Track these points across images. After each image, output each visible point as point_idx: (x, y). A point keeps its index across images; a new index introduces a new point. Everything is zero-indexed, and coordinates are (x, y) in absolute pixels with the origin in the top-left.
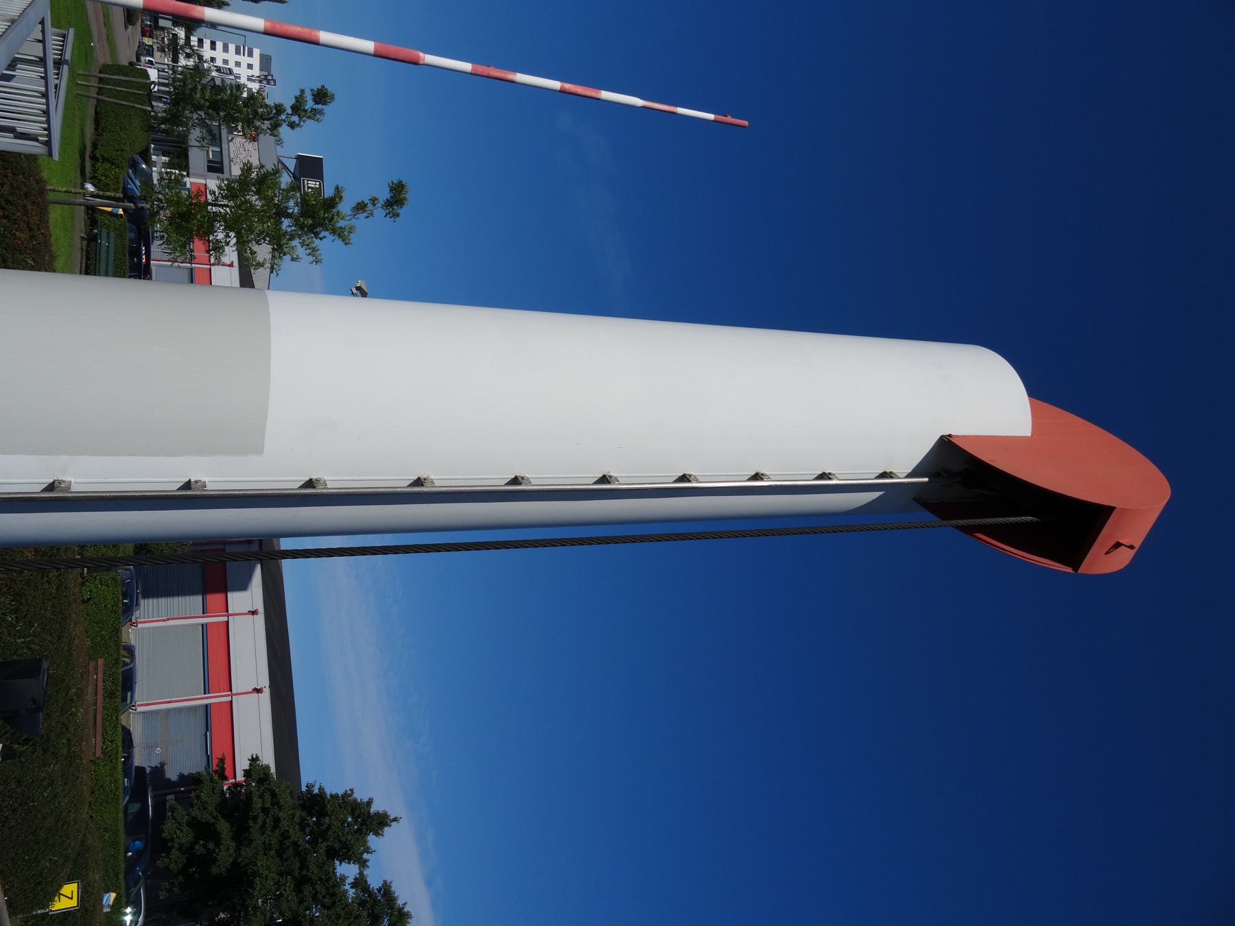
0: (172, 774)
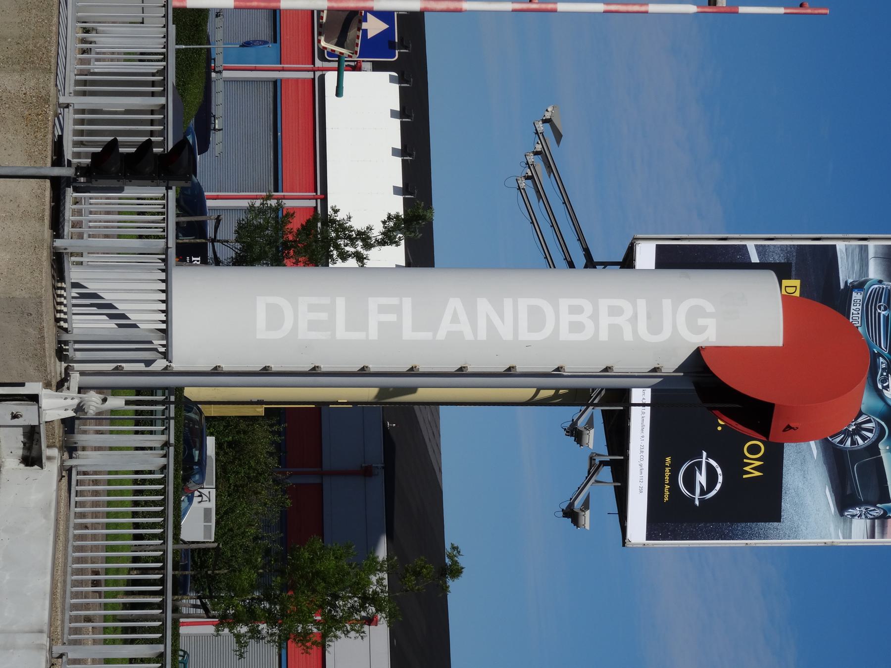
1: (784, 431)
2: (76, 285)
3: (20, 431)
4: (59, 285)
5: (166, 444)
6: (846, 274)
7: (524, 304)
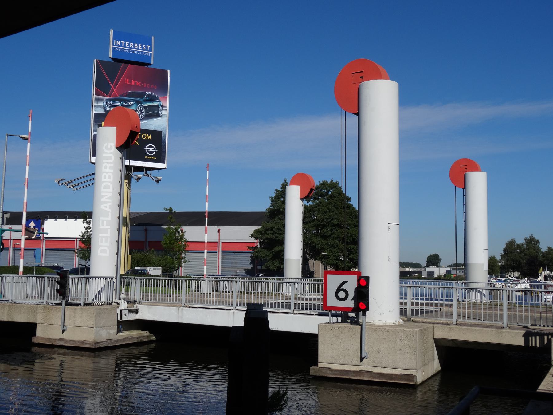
0: (250, 267)
1: (137, 128)
2: (93, 300)
3: (129, 314)
4: (93, 304)
5: (134, 278)
6: (102, 111)
7: (103, 190)
